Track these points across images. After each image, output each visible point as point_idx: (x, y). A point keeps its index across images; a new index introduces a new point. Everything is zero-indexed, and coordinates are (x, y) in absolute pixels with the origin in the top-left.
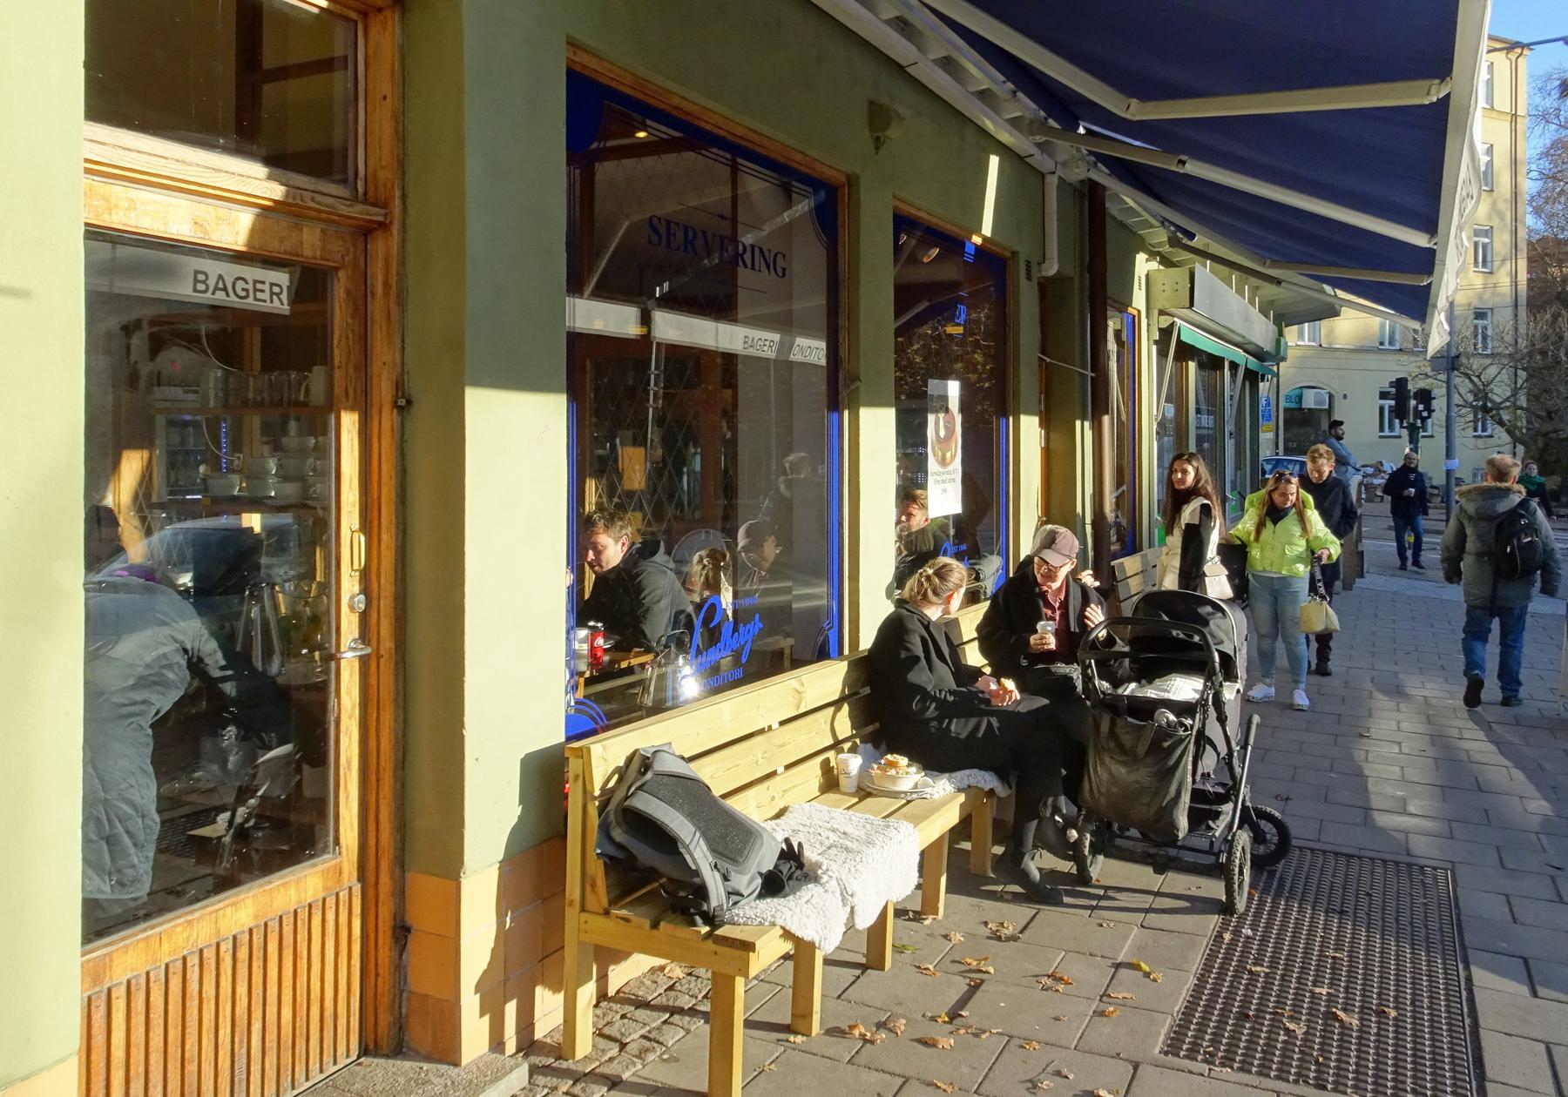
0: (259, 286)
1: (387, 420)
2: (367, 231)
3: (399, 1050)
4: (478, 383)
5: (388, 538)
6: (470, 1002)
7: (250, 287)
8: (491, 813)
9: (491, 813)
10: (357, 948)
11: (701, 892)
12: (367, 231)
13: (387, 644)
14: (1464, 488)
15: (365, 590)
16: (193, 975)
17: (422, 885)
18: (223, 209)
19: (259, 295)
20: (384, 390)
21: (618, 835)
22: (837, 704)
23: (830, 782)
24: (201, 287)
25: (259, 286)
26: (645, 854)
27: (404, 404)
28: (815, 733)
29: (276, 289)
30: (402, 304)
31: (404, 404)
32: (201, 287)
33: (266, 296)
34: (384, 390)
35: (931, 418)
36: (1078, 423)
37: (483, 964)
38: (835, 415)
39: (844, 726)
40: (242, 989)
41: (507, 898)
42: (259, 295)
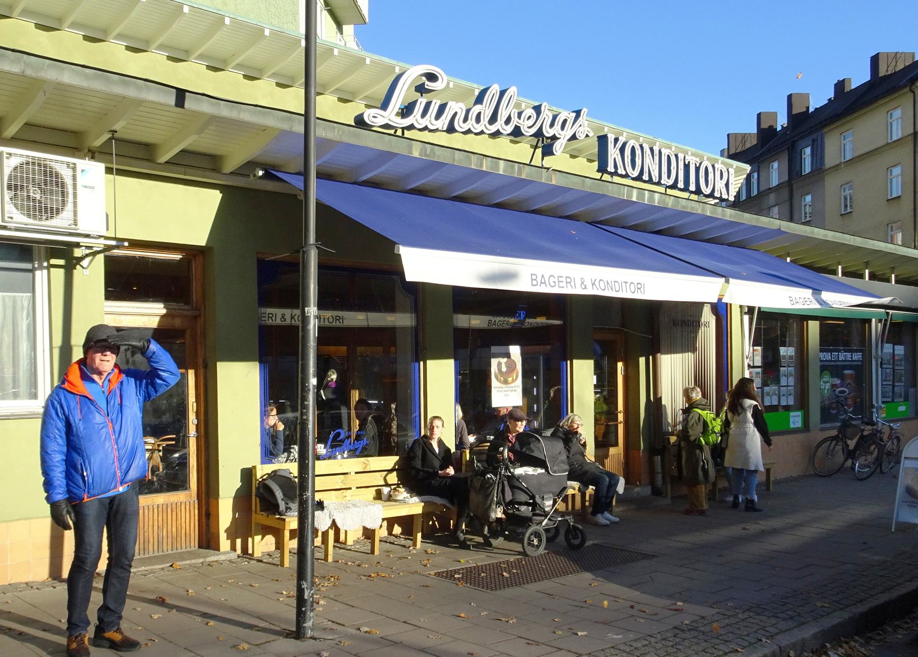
0: (560, 279)
1: (202, 371)
2: (196, 318)
3: (208, 547)
4: (222, 360)
5: (202, 404)
6: (223, 536)
7: (556, 280)
8: (229, 485)
9: (229, 485)
10: (197, 518)
11: (278, 506)
12: (196, 318)
13: (203, 433)
14: (757, 383)
15: (197, 418)
16: (146, 511)
17: (212, 501)
18: (151, 318)
19: (561, 284)
20: (200, 361)
21: (261, 490)
22: (390, 471)
23: (379, 496)
24: (534, 282)
25: (560, 279)
26: (267, 495)
27: (206, 366)
28: (378, 479)
29: (569, 280)
30: (205, 337)
31: (206, 366)
32: (534, 282)
33: (564, 284)
34: (200, 361)
35: (494, 362)
36: (642, 360)
37: (228, 525)
38: (417, 364)
39: (393, 478)
40: (160, 518)
41: (235, 509)
42: (561, 284)
